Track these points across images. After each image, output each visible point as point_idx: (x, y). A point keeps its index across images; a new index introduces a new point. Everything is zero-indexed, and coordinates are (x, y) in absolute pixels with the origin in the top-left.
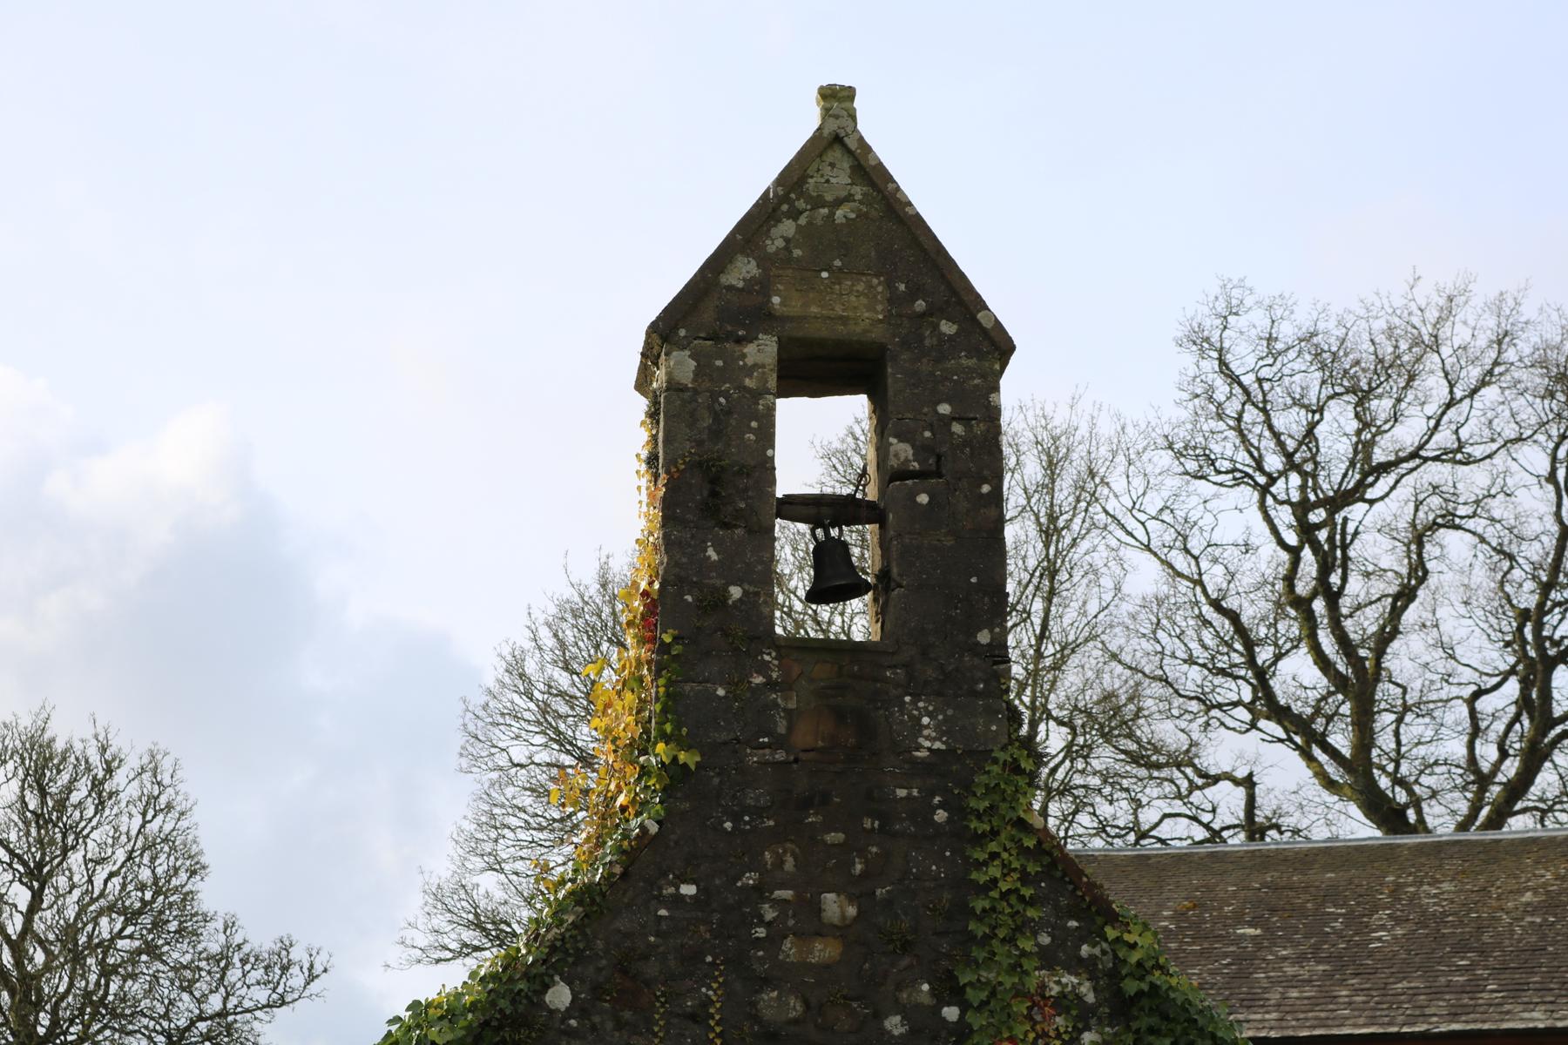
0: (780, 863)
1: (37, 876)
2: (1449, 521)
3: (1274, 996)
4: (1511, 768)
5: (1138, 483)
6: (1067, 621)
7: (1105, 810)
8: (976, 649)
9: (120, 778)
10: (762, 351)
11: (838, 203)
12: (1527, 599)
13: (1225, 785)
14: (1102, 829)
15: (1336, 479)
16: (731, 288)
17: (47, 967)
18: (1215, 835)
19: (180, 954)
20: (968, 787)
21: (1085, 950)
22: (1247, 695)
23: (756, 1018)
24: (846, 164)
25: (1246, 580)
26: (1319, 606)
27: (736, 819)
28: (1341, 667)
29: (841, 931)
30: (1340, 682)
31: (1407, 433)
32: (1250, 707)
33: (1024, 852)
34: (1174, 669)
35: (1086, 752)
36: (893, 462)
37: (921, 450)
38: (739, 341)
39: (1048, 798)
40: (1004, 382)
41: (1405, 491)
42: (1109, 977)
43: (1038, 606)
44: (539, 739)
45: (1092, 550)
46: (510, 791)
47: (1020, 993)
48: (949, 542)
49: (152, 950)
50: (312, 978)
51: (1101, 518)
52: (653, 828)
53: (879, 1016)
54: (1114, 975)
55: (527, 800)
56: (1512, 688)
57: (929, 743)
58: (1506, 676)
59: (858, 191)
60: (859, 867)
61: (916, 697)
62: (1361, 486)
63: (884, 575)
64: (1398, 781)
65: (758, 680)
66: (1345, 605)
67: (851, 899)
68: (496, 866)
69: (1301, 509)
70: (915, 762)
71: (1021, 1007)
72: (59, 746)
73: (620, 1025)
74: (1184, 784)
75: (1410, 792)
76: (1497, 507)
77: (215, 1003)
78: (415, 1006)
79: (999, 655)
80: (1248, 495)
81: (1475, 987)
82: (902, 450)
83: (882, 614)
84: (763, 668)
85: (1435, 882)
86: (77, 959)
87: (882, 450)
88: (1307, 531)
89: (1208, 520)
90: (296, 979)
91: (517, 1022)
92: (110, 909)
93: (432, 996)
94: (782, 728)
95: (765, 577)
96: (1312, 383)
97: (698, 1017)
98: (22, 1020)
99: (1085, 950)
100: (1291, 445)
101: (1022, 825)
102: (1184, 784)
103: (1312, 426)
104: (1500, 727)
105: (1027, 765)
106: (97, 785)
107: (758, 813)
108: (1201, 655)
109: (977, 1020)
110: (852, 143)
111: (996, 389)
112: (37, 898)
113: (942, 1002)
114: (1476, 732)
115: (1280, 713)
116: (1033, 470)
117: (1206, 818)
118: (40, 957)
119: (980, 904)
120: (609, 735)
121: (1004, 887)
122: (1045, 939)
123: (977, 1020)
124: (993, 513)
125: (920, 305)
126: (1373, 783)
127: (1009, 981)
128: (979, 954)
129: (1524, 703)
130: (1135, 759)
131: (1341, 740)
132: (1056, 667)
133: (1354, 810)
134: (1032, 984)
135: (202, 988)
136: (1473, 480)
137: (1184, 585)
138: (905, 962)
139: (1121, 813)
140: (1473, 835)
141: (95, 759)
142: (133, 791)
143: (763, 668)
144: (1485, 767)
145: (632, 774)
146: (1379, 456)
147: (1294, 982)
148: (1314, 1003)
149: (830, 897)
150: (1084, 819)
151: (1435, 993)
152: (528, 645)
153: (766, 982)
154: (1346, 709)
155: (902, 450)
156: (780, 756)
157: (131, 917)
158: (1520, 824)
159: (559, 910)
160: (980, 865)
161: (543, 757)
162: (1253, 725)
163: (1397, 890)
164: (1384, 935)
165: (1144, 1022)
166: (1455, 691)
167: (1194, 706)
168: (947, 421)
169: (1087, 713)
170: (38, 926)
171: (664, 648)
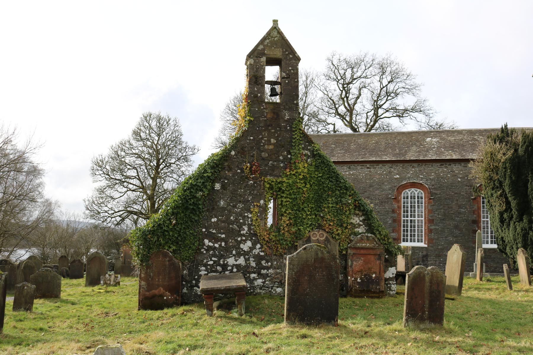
0: (265, 134)
1: (159, 135)
2: (365, 87)
3: (337, 155)
4: (372, 123)
5: (319, 80)
6: (309, 101)
7: (313, 128)
8: (294, 104)
9: (170, 122)
10: (264, 59)
11: (275, 37)
12: (376, 99)
13: (331, 125)
14: (313, 131)
15: (348, 80)
16: (259, 50)
17: (160, 149)
18: (329, 132)
19: (179, 147)
20: (293, 124)
21: (309, 148)
22: (334, 112)
23: (261, 157)
24: (276, 31)
25: (335, 95)
26: (345, 99)
27: (259, 128)
28: (348, 108)
29: (274, 144)
30: (348, 110)
31: (359, 74)
32: (335, 114)
33: (300, 133)
34: (324, 108)
35: (311, 120)
36: (283, 76)
37: (287, 74)
38: (260, 58)
39: (305, 126)
40: (299, 64)
41: (359, 82)
42: (312, 152)
43: (304, 98)
44: (231, 117)
45: (312, 90)
46: (227, 124)
47: (299, 154)
48: (290, 88)
49: (175, 146)
50: (198, 151)
51: (314, 86)
52: (247, 129)
53: (279, 156)
54: (313, 151)
55: (229, 125)
56: (373, 111)
57: (287, 117)
58: (372, 110)
59: (278, 36)
60: (276, 135)
61: (285, 111)
62: (352, 81)
63: (281, 93)
64: (356, 125)
65: (262, 108)
66: (349, 99)
67: (275, 140)
68: (225, 135)
69: (343, 85)
70: (285, 120)
71: (299, 156)
72: (162, 117)
73: (242, 157)
74: (325, 125)
75: (357, 126)
76: (372, 85)
77: (184, 154)
78: (212, 154)
79: (297, 104)
80: (335, 83)
81: (365, 154)
82: (284, 74)
83: (280, 98)
84: (263, 106)
85: (360, 139)
86: (165, 147)
87: (281, 74)
88: (344, 88)
89: (329, 86)
90: (196, 151)
91: (227, 156)
92: (169, 140)
93: (215, 153)
94: (266, 115)
95: (263, 92)
96: (345, 66)
97: (253, 156)
98: (157, 156)
99: (309, 148)
100: (342, 75)
101: (300, 129)
102: (325, 125)
103: (345, 73)
104: (371, 117)
105: (301, 121)
106: (167, 123)
107: (262, 127)
108: (328, 106)
109: (293, 157)
110: (277, 28)
111: (298, 65)
112: (159, 138)
113: (288, 155)
114: (367, 118)
115: (339, 115)
116: (304, 78)
117: (328, 130)
118: (159, 147)
119: (294, 141)
120: (240, 115)
121: (297, 138)
122: (303, 146)
123: (293, 157)
124: (297, 84)
125: (287, 53)
126: (352, 125)
127: (298, 152)
128: (293, 148)
129: (374, 114)
130: (318, 121)
131: (348, 118)
132: (307, 107)
133: (349, 129)
134: (301, 152)
135: (182, 152)
136: (368, 81)
137: (326, 96)
138: (283, 149)
139: (315, 129)
140: (366, 133)
141: (167, 119)
142: (172, 123)
143: (263, 106)
144: (368, 123)
145: (244, 121)
146: (355, 77)
147: (340, 153)
148: (342, 156)
149: (272, 140)
150: (310, 129)
151: (359, 155)
152: (230, 103)
153: (263, 151)
154: (348, 114)
155: (284, 74)
156: (265, 119)
157: (172, 141)
158: (373, 131)
159: (233, 141)
160: (294, 135)
161: (232, 119)
162: (335, 116)
163: (355, 140)
164: (353, 147)
165: (317, 158)
166: (364, 112)
167: (327, 113)
168: (290, 70)
169: (311, 114)
170: (159, 143)
171: (249, 103)
